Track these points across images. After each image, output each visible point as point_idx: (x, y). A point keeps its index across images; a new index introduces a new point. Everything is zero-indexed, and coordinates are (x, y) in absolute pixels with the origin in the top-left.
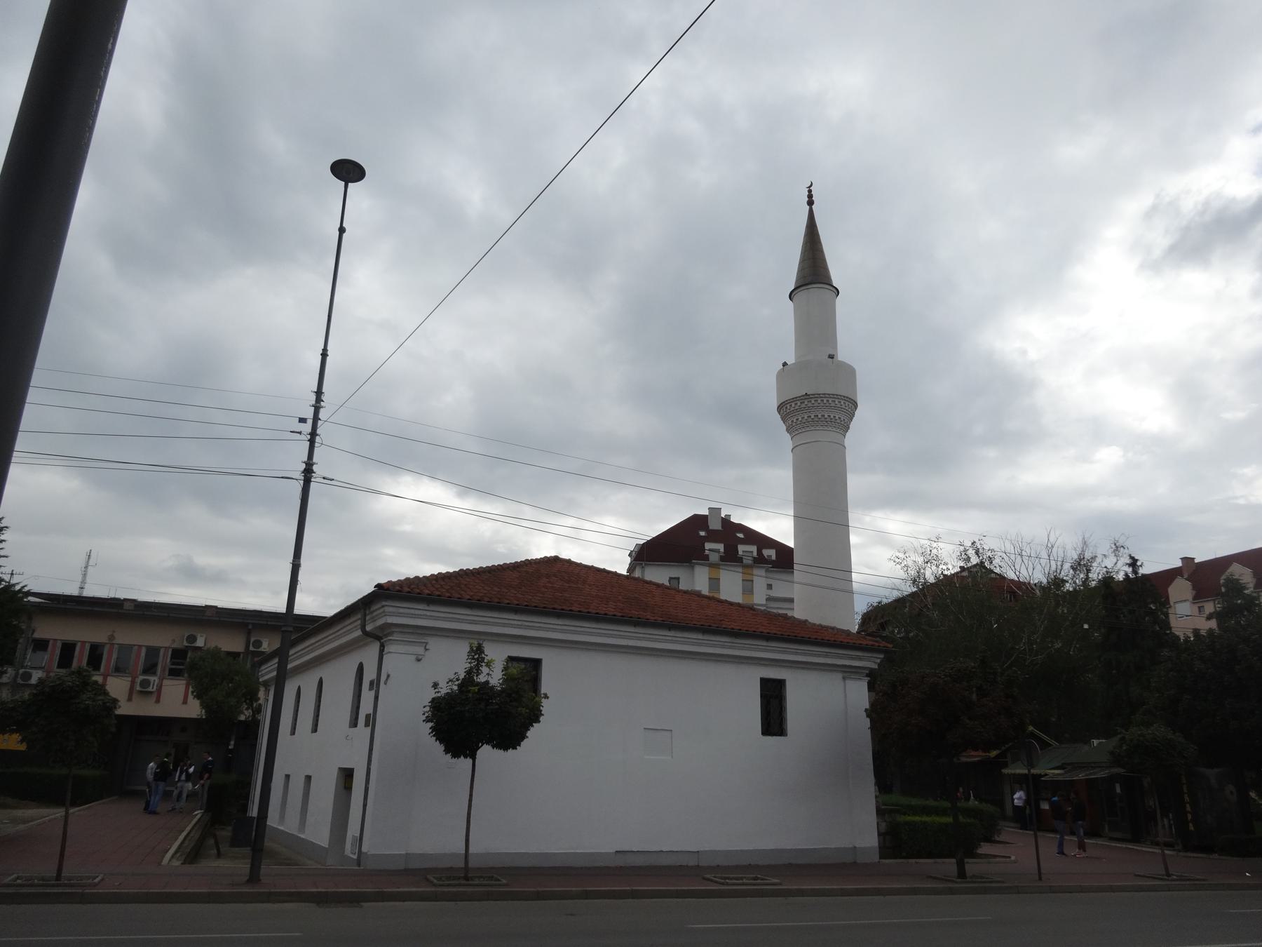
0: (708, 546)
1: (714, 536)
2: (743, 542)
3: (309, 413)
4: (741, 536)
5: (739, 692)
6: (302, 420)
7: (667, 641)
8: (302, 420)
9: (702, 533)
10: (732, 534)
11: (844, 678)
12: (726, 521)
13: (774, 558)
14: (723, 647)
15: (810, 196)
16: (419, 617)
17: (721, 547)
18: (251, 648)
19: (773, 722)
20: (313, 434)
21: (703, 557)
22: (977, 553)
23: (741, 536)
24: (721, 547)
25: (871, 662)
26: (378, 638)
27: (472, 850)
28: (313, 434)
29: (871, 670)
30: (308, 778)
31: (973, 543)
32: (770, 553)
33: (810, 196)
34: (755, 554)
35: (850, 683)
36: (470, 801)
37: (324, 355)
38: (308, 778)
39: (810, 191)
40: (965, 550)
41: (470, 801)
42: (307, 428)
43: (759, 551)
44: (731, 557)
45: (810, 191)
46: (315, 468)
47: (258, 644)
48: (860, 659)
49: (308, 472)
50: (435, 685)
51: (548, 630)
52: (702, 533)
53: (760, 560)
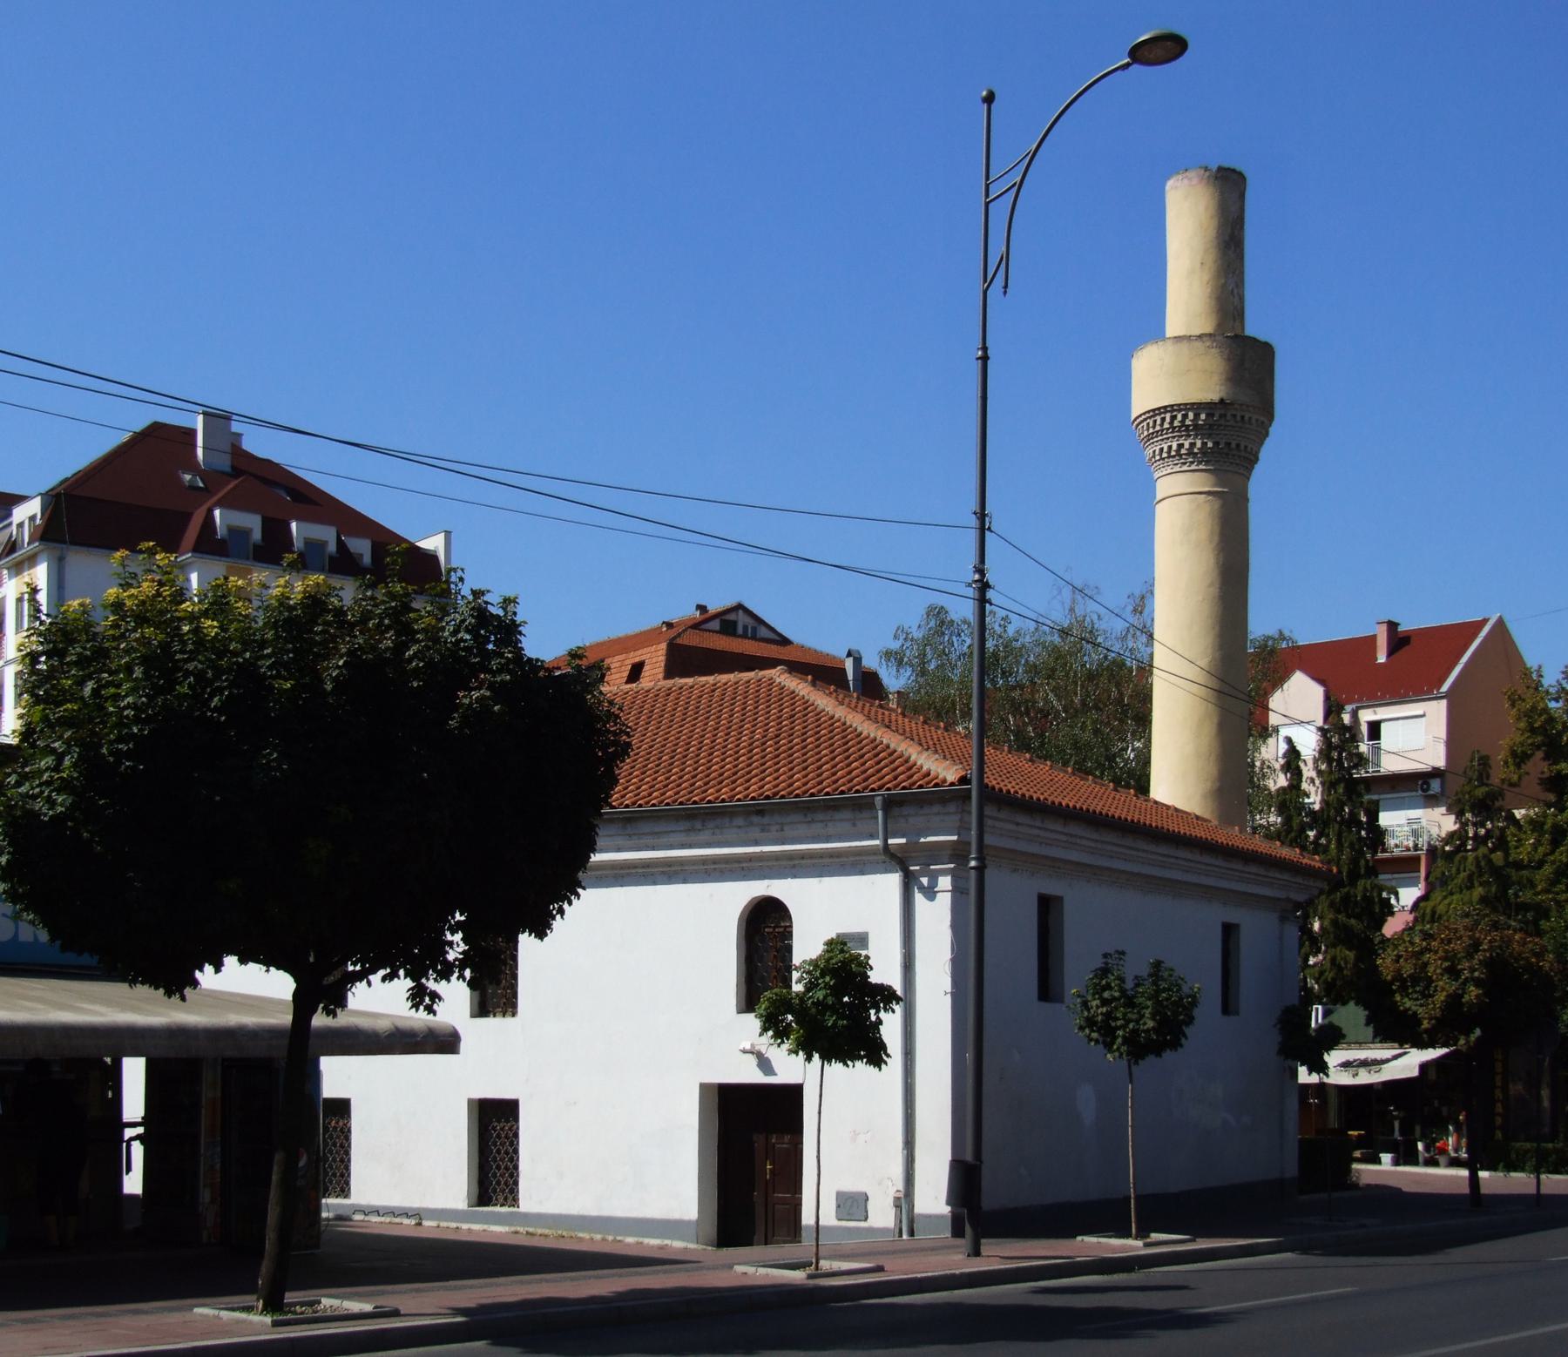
13: (367, 559)
17: (252, 523)
24: (252, 523)
32: (361, 547)
34: (332, 547)
43: (340, 544)
44: (273, 549)
53: (343, 563)
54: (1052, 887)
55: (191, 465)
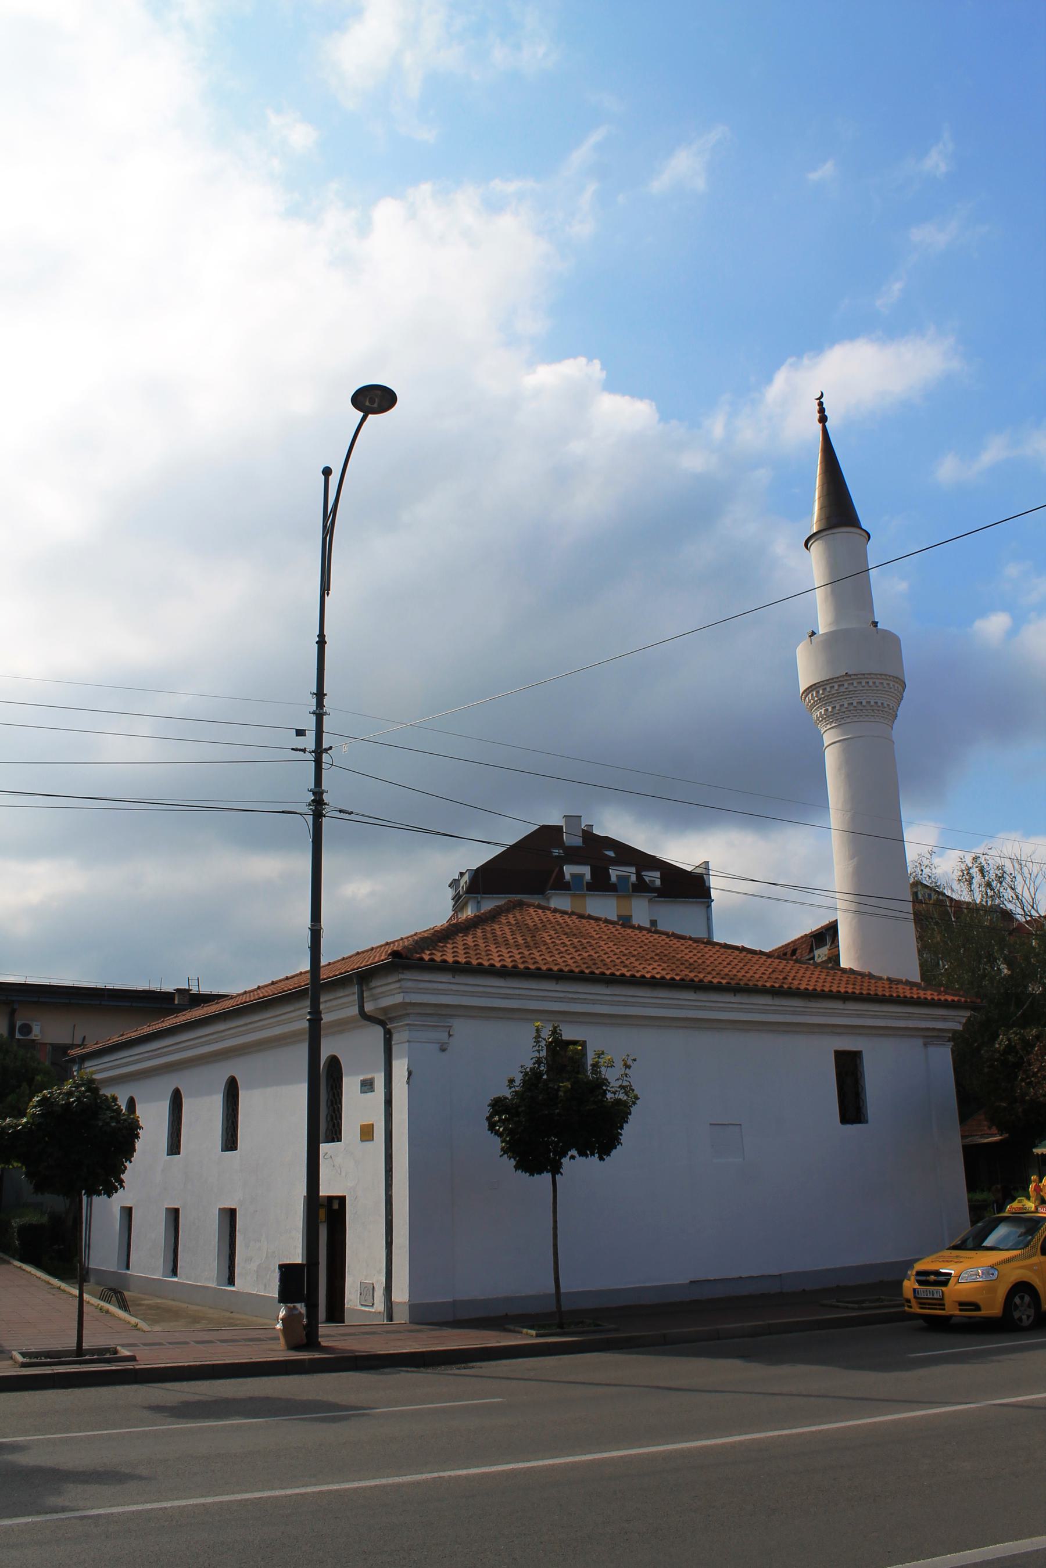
0: (569, 870)
1: (574, 856)
2: (618, 862)
3: (309, 723)
4: (611, 854)
5: (808, 1065)
6: (300, 733)
7: (732, 1010)
8: (300, 733)
9: (556, 852)
10: (603, 855)
11: (925, 1045)
12: (588, 836)
13: (658, 882)
14: (794, 1013)
15: (822, 410)
16: (444, 992)
17: (586, 871)
18: (18, 1036)
19: (852, 1107)
20: (319, 751)
21: (562, 885)
22: (982, 871)
23: (611, 854)
24: (586, 871)
25: (955, 1021)
26: (382, 1023)
27: (562, 1290)
28: (319, 751)
29: (955, 1032)
30: (174, 1215)
31: (975, 859)
32: (654, 877)
33: (822, 410)
34: (633, 878)
35: (931, 1049)
36: (555, 1228)
37: (321, 642)
38: (174, 1215)
39: (821, 404)
40: (969, 869)
41: (555, 1228)
42: (309, 741)
43: (639, 876)
44: (600, 884)
45: (821, 404)
46: (326, 797)
47: (27, 1029)
48: (944, 1019)
49: (318, 804)
50: (511, 1081)
51: (594, 1002)
52: (556, 852)
53: (641, 887)
54: (848, 1044)
55: (560, 843)
